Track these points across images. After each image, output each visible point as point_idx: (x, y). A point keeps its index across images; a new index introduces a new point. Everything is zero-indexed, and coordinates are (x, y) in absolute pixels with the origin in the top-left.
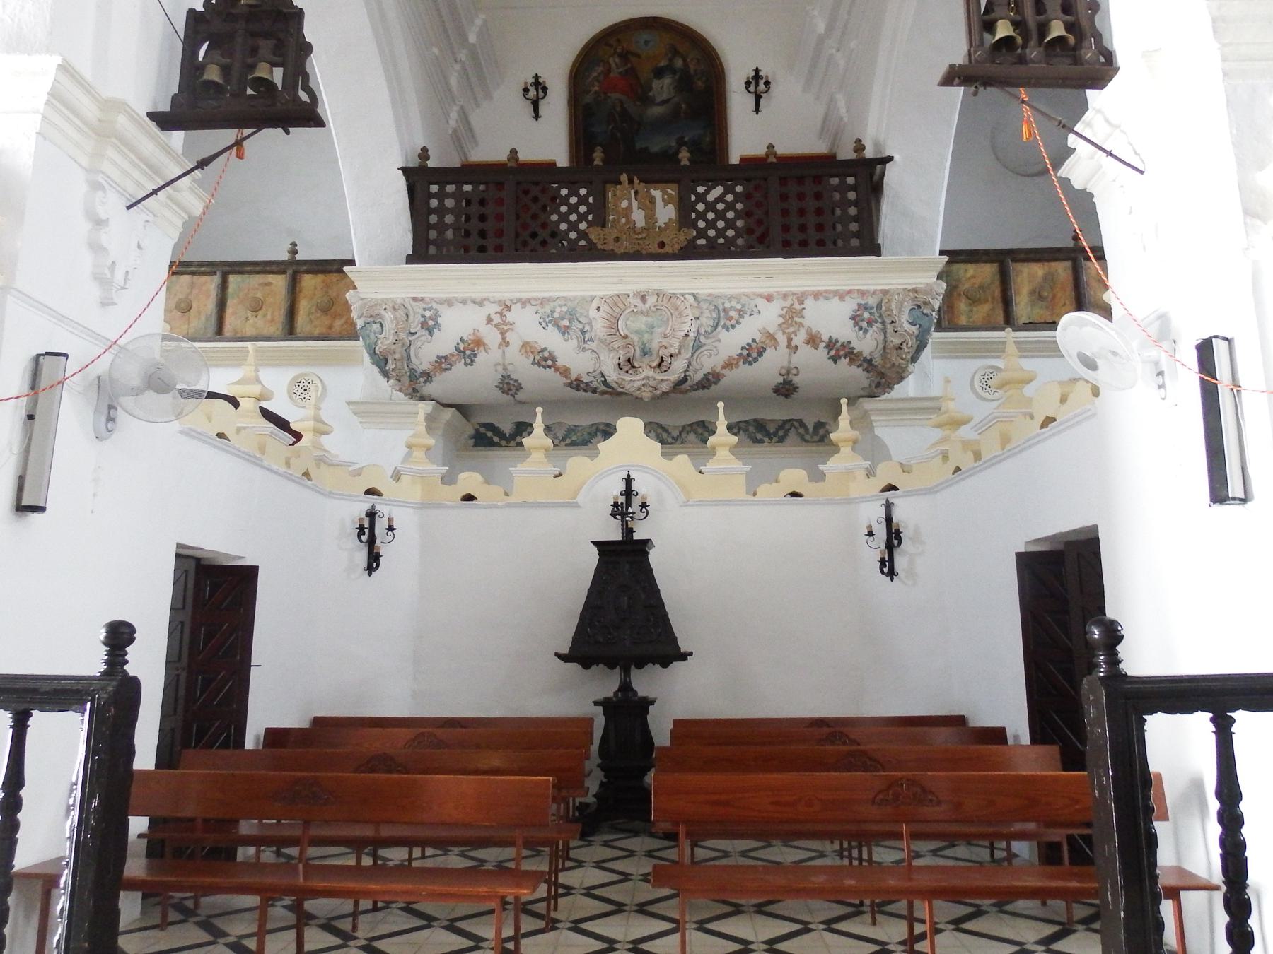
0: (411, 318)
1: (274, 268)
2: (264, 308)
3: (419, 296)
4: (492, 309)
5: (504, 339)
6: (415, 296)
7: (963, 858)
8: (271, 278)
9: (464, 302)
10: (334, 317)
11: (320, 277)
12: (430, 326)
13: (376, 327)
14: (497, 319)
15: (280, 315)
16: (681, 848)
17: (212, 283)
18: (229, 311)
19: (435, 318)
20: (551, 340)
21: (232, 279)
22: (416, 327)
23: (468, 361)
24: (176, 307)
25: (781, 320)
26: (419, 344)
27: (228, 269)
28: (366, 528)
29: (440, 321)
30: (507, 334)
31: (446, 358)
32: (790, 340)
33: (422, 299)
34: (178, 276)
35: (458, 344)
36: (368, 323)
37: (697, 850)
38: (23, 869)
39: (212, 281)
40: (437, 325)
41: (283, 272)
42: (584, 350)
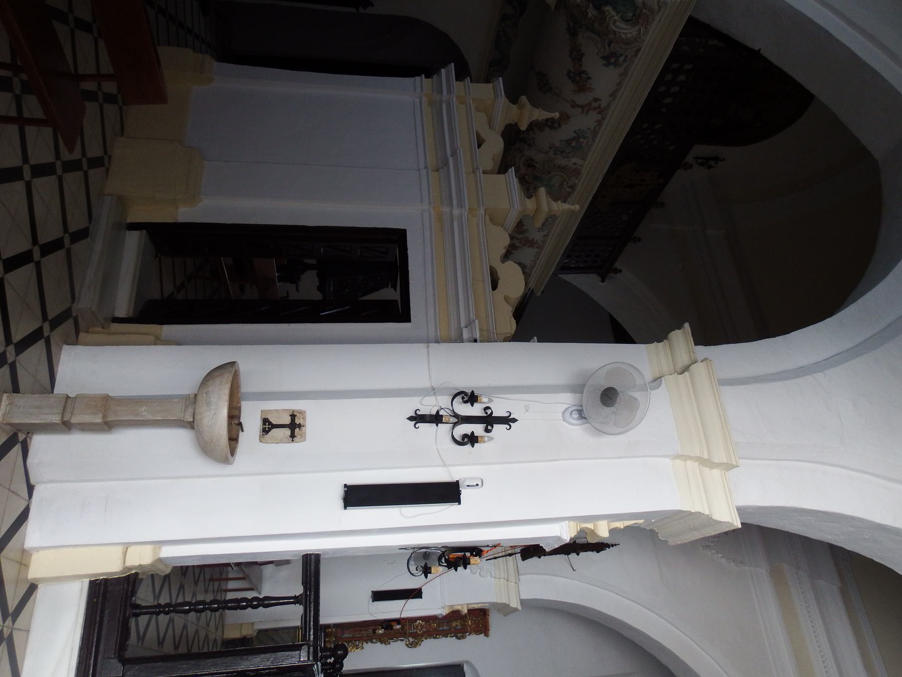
4: (604, 104)
5: (578, 106)
6: (641, 51)
7: (59, 545)
9: (619, 84)
12: (610, 59)
13: (630, 15)
14: (596, 104)
16: (128, 604)
19: (616, 64)
20: (566, 132)
23: (571, 75)
25: (530, 239)
30: (580, 109)
31: (580, 60)
32: (517, 239)
33: (636, 55)
35: (587, 74)
36: (635, 10)
37: (146, 617)
38: (31, 615)
40: (608, 64)
42: (550, 148)
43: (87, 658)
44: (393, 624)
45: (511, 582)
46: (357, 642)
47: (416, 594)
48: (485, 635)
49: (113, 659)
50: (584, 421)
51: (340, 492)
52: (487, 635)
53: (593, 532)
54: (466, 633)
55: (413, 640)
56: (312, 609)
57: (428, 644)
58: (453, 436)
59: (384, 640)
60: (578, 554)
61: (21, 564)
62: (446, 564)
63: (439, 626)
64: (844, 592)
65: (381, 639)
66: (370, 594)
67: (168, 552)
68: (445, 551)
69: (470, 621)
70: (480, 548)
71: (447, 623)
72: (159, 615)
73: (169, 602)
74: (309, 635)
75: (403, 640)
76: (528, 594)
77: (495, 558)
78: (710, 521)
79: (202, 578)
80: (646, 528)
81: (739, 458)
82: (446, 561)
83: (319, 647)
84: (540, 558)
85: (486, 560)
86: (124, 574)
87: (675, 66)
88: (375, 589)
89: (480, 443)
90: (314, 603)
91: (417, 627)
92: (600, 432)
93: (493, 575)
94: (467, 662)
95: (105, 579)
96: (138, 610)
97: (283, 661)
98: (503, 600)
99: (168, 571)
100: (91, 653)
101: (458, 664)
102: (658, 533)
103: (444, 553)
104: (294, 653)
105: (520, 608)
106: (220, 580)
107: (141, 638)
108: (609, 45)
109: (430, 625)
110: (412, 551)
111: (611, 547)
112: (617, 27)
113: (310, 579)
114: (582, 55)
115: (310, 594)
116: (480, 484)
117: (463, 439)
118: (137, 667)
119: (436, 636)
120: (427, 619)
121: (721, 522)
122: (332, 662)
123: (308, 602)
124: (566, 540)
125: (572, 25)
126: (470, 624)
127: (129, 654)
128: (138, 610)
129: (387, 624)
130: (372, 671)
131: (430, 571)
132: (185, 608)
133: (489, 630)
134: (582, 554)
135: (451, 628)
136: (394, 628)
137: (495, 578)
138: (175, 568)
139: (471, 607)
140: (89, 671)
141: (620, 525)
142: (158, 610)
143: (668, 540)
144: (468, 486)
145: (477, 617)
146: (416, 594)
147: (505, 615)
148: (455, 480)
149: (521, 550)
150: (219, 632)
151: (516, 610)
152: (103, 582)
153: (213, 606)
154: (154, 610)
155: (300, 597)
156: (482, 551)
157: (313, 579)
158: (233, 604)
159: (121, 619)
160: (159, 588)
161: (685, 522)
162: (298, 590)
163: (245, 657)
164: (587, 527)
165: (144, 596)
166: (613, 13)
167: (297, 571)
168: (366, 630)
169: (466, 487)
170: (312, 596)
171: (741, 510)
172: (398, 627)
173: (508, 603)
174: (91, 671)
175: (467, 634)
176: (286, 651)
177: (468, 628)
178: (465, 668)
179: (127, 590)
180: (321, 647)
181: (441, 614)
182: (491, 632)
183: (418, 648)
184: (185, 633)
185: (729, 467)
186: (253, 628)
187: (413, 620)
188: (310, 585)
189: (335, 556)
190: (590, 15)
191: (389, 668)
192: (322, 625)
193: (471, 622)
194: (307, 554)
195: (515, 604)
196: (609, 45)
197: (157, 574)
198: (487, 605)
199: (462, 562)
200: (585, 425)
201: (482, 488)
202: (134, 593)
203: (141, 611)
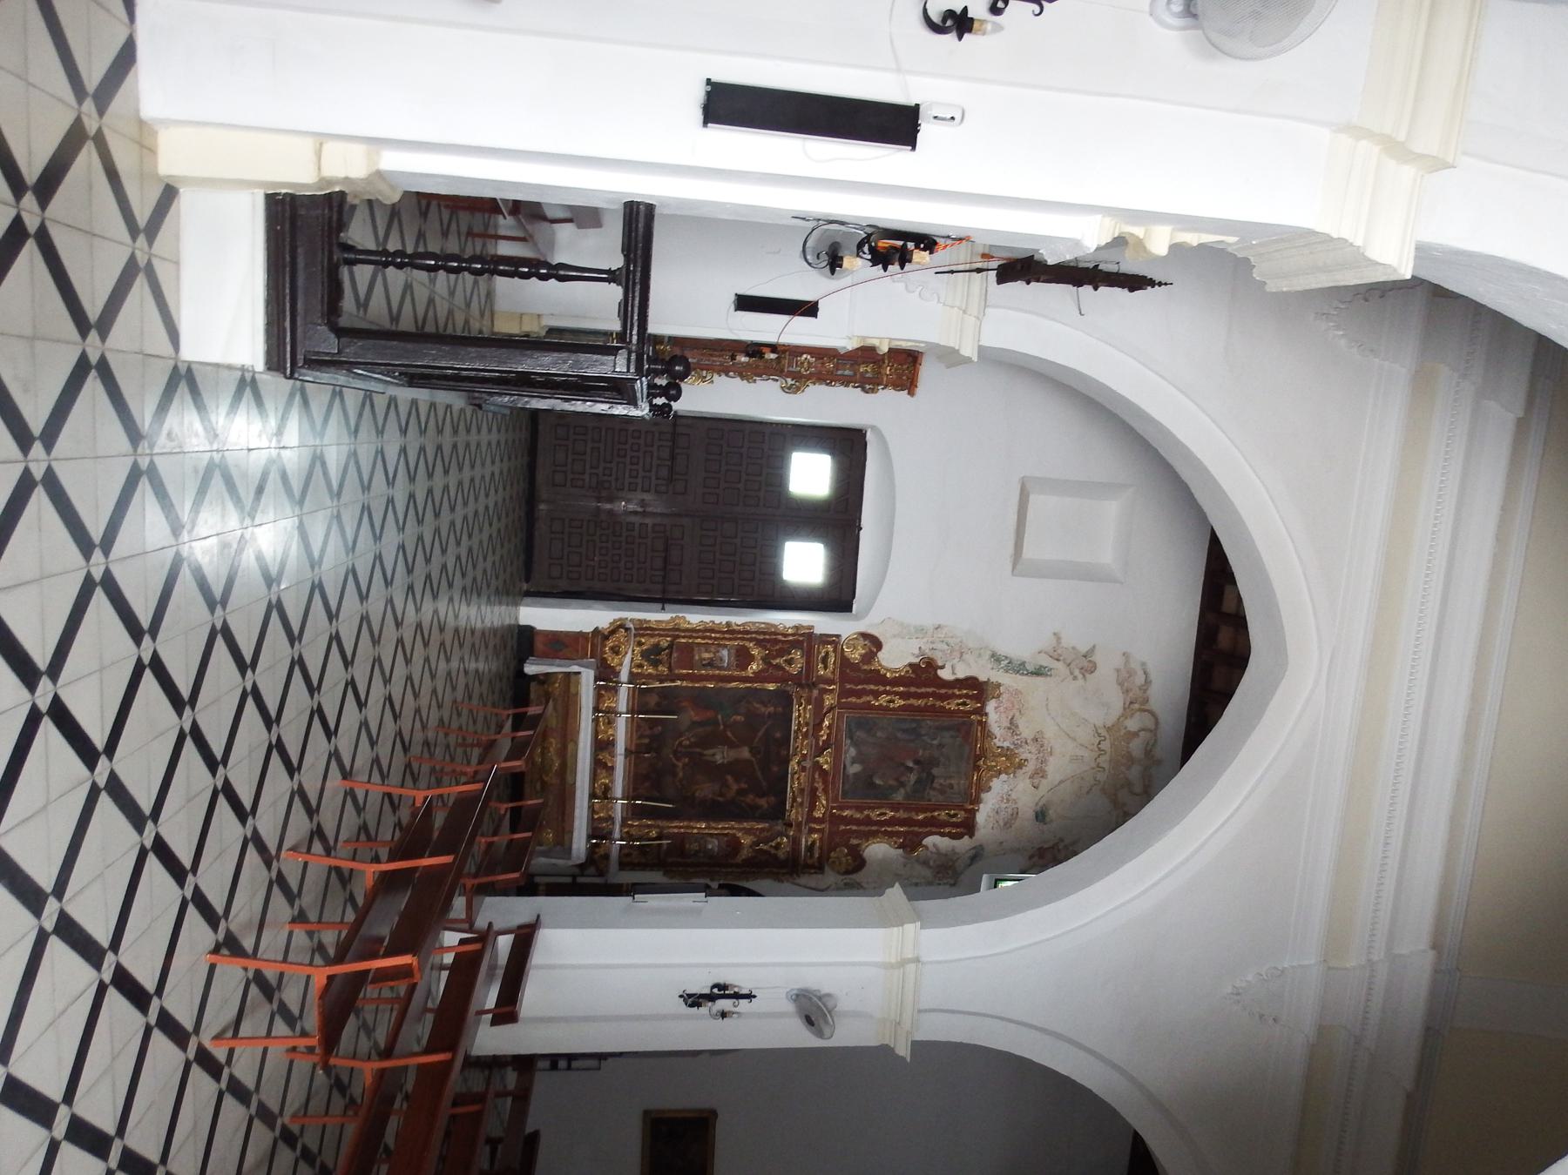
37: (370, 268)
43: (279, 319)
44: (765, 350)
45: (970, 315)
46: (705, 372)
47: (808, 309)
48: (909, 393)
49: (321, 325)
50: (1189, 21)
51: (698, 94)
52: (911, 393)
53: (1140, 244)
54: (878, 385)
55: (793, 382)
56: (637, 294)
57: (815, 391)
58: (925, 10)
59: (746, 374)
60: (1096, 289)
61: (142, 146)
62: (869, 257)
63: (837, 367)
64: (1522, 426)
65: (742, 373)
66: (733, 298)
67: (393, 161)
68: (871, 234)
69: (889, 368)
70: (935, 238)
71: (852, 365)
72: (387, 267)
73: (400, 248)
74: (631, 335)
75: (777, 380)
76: (992, 340)
77: (952, 272)
78: (1359, 259)
79: (454, 226)
80: (1236, 253)
81: (1465, 153)
82: (873, 250)
83: (645, 356)
84: (1028, 284)
85: (936, 273)
86: (322, 189)
88: (741, 292)
89: (975, 33)
90: (641, 284)
91: (802, 363)
92: (1216, 49)
93: (942, 300)
94: (873, 428)
95: (291, 194)
96: (354, 256)
97: (587, 368)
98: (950, 341)
99: (396, 198)
100: (284, 312)
101: (858, 427)
102: (1254, 266)
103: (869, 236)
104: (606, 358)
105: (975, 359)
106: (485, 236)
107: (363, 305)
109: (823, 364)
110: (815, 223)
111: (1157, 287)
113: (636, 245)
115: (635, 271)
116: (958, 117)
117: (944, 20)
118: (360, 344)
119: (831, 382)
120: (821, 354)
121: (1377, 263)
122: (664, 385)
123: (631, 283)
124: (1089, 249)
126: (888, 373)
127: (344, 322)
128: (354, 256)
129: (754, 350)
131: (840, 263)
132: (428, 262)
133: (916, 386)
134: (1102, 289)
135: (855, 374)
136: (766, 356)
137: (944, 304)
138: (407, 194)
139: (895, 344)
140: (285, 338)
141: (1193, 239)
142: (384, 259)
143: (1267, 281)
144: (935, 117)
145: (901, 365)
146: (808, 309)
147: (948, 367)
148: (912, 102)
149: (999, 266)
150: (486, 322)
151: (968, 360)
152: (288, 199)
153: (474, 266)
154: (378, 258)
155: (617, 273)
156: (935, 243)
157: (641, 245)
158: (507, 268)
159: (326, 264)
160: (385, 227)
161: (1311, 253)
162: (616, 262)
163: (529, 352)
164: (1132, 232)
165: (359, 234)
167: (613, 234)
168: (720, 356)
169: (932, 120)
170: (638, 274)
171: (1423, 252)
172: (773, 356)
173: (957, 348)
174: (288, 339)
175: (880, 387)
176: (594, 354)
177: (882, 379)
178: (869, 436)
179: (330, 218)
180: (648, 355)
181: (845, 348)
182: (920, 390)
183: (799, 395)
184: (431, 314)
185: (1437, 164)
186: (539, 323)
187: (796, 351)
188: (635, 255)
189: (678, 213)
191: (750, 417)
192: (650, 335)
193: (890, 370)
194: (632, 201)
195: (968, 350)
197: (377, 199)
198: (923, 345)
199: (898, 256)
200: (1188, 32)
201: (963, 125)
202: (342, 225)
203: (358, 257)
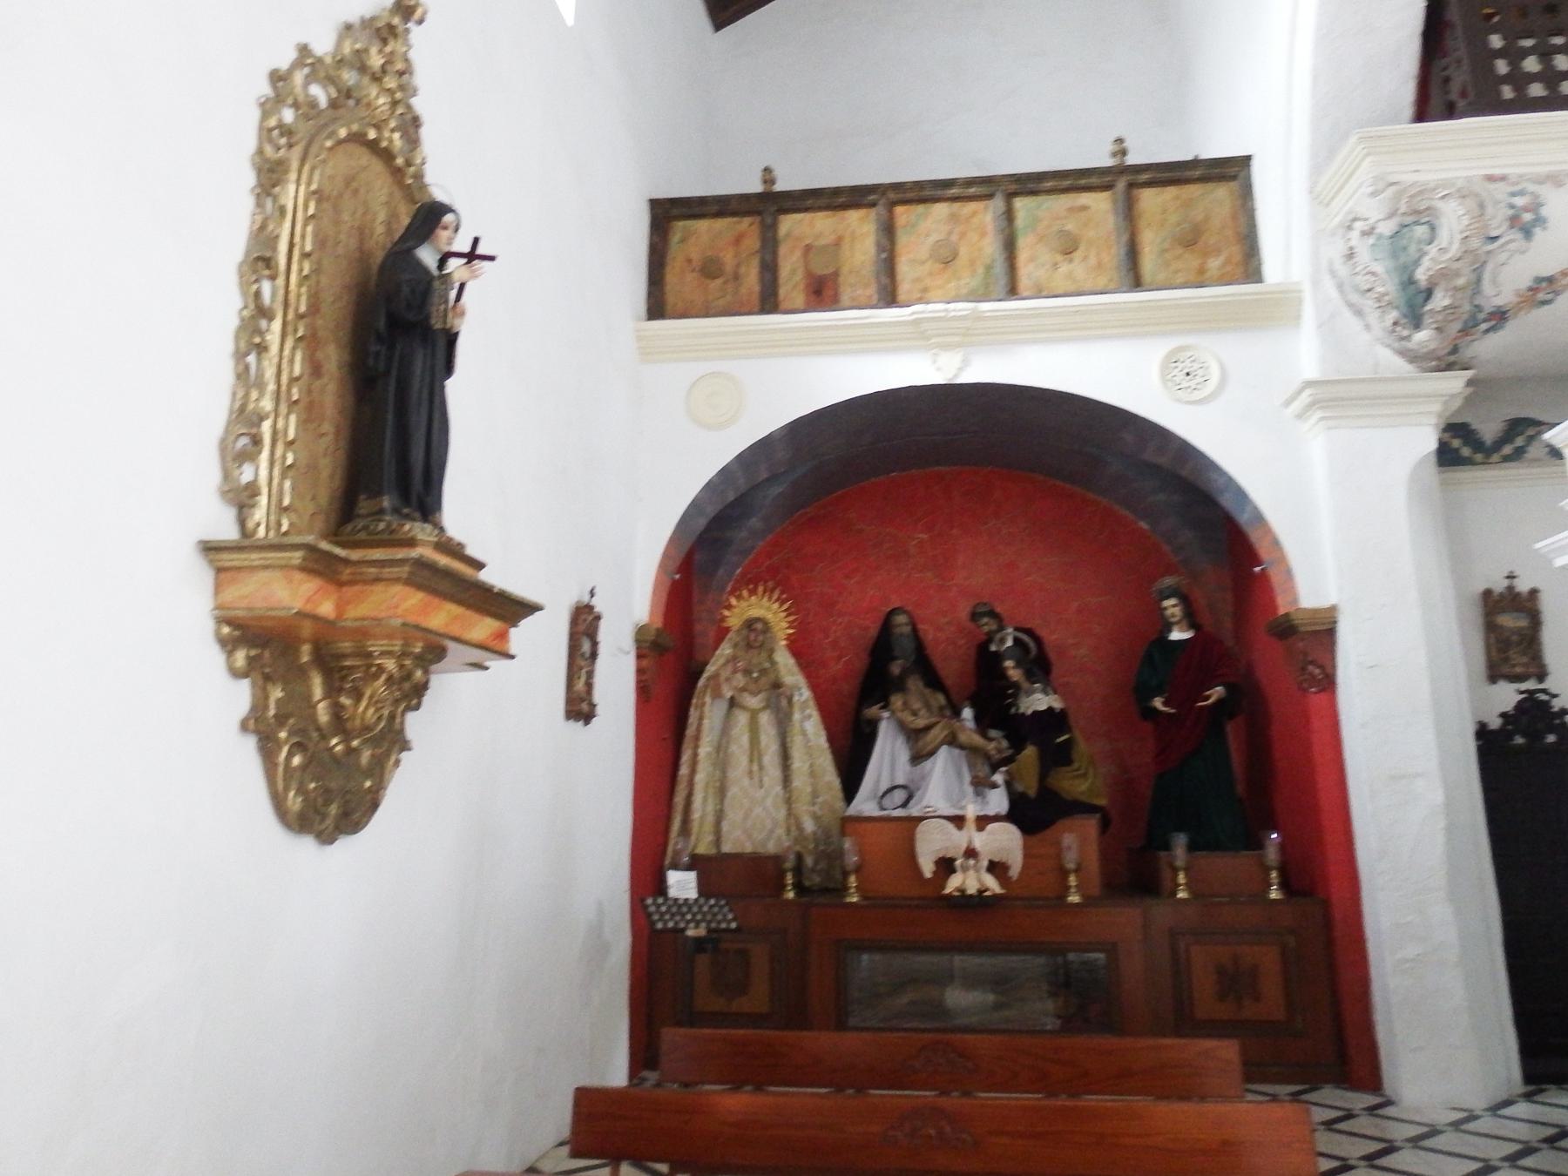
0: (1490, 210)
1: (1094, 180)
2: (1082, 248)
3: (1497, 172)
8: (1085, 199)
10: (1206, 254)
11: (1171, 192)
12: (1526, 223)
13: (1421, 231)
15: (1113, 254)
17: (986, 214)
18: (1023, 256)
19: (1535, 207)
21: (1020, 203)
22: (1499, 227)
24: (931, 256)
26: (1503, 257)
27: (1013, 187)
28: (305, 641)
29: (1544, 212)
31: (1550, 280)
33: (1503, 178)
34: (928, 205)
39: (986, 208)
40: (1540, 221)
41: (1108, 187)
87: (1507, 92)
108: (1495, 238)
112: (1451, 243)
114: (1539, 280)
125: (1484, 326)
130: (895, 350)
166: (1426, 262)
190: (1447, 302)
196: (1495, 238)
